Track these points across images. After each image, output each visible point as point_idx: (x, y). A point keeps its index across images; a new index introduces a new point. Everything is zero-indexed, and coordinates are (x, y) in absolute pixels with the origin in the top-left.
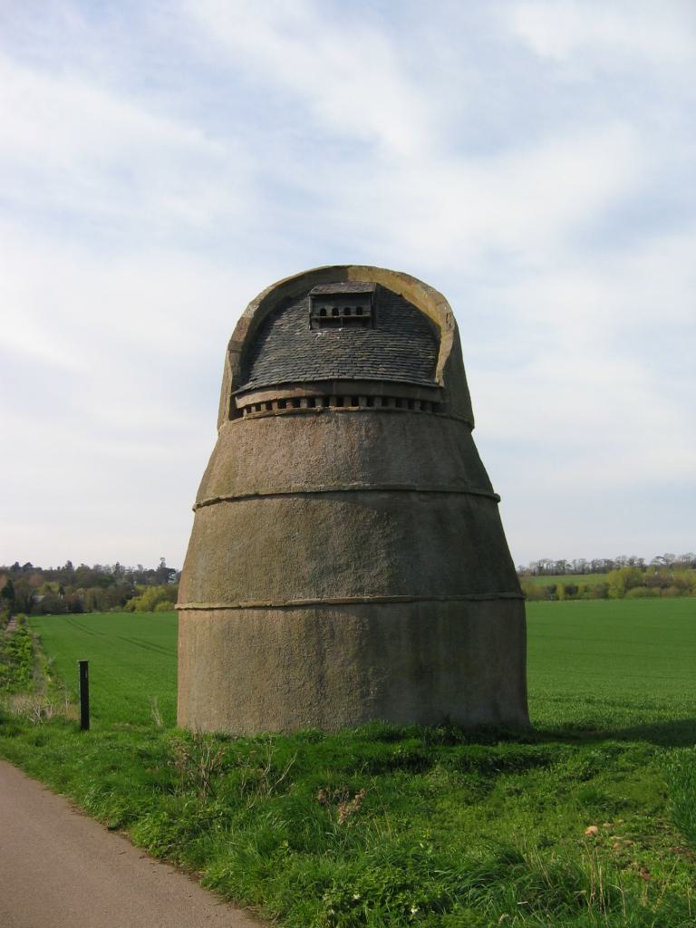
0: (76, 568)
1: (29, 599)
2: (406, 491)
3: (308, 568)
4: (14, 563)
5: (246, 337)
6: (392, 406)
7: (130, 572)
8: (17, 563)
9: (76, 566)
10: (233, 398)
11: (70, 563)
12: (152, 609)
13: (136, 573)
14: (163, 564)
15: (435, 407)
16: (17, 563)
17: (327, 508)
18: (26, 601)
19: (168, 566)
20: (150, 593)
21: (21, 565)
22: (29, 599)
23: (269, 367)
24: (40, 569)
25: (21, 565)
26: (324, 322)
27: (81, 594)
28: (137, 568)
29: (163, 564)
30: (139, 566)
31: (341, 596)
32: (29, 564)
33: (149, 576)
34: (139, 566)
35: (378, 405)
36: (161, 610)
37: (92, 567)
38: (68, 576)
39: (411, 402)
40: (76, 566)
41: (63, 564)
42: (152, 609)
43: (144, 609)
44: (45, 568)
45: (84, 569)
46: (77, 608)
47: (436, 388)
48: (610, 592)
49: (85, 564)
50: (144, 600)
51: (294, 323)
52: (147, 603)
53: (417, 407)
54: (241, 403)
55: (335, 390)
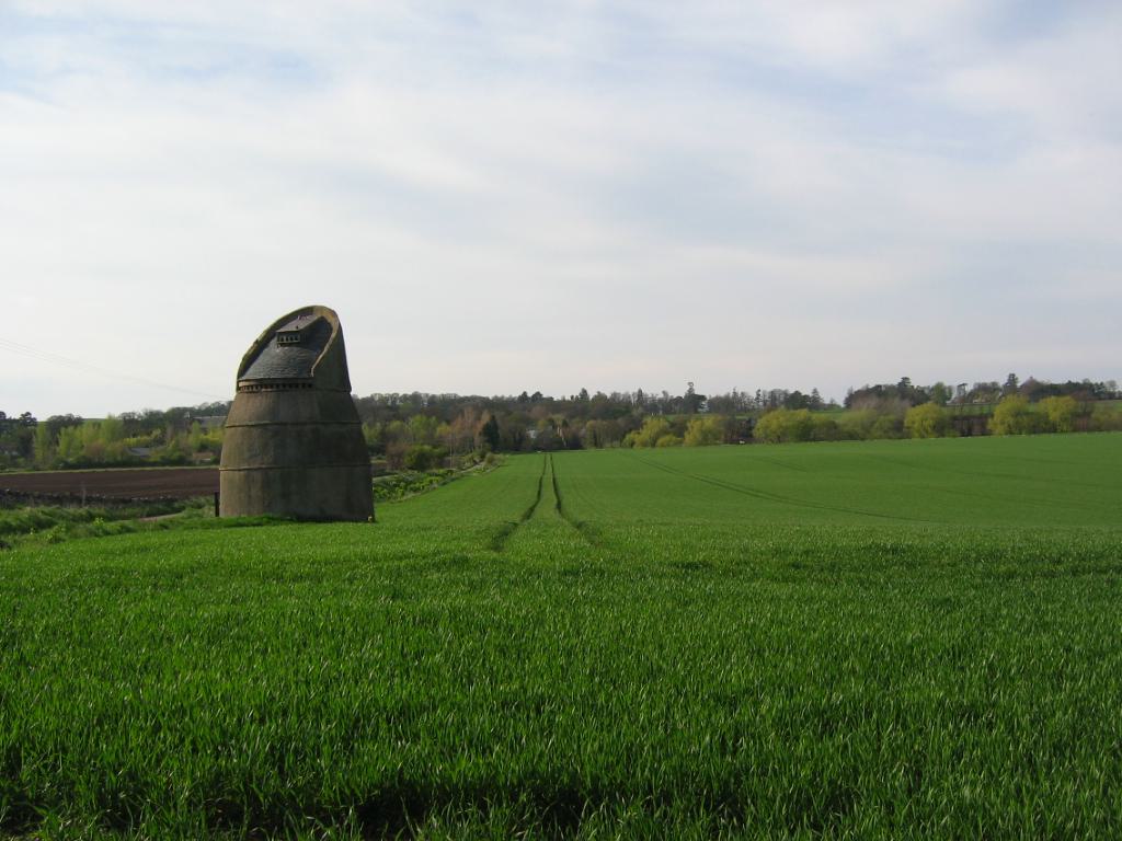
0: (591, 398)
1: (517, 435)
2: (285, 424)
3: (247, 455)
4: (521, 393)
5: (306, 328)
6: (287, 388)
7: (653, 399)
8: (525, 393)
9: (592, 394)
10: (238, 383)
11: (584, 391)
12: (654, 444)
13: (660, 400)
14: (691, 390)
15: (310, 386)
16: (525, 393)
17: (255, 432)
18: (514, 437)
19: (698, 392)
20: (652, 424)
21: (530, 395)
22: (517, 435)
23: (252, 373)
24: (538, 395)
25: (530, 395)
26: (283, 345)
27: (585, 429)
28: (661, 396)
29: (691, 390)
30: (664, 392)
31: (256, 466)
32: (538, 394)
33: (676, 404)
34: (664, 392)
35: (281, 387)
36: (663, 446)
37: (609, 395)
38: (581, 407)
39: (297, 386)
40: (592, 394)
41: (577, 393)
42: (654, 444)
43: (644, 445)
44: (557, 397)
45: (600, 397)
46: (575, 444)
47: (311, 378)
48: (990, 424)
49: (602, 392)
50: (646, 433)
51: (275, 350)
52: (647, 437)
53: (300, 386)
54: (241, 384)
55: (265, 382)
